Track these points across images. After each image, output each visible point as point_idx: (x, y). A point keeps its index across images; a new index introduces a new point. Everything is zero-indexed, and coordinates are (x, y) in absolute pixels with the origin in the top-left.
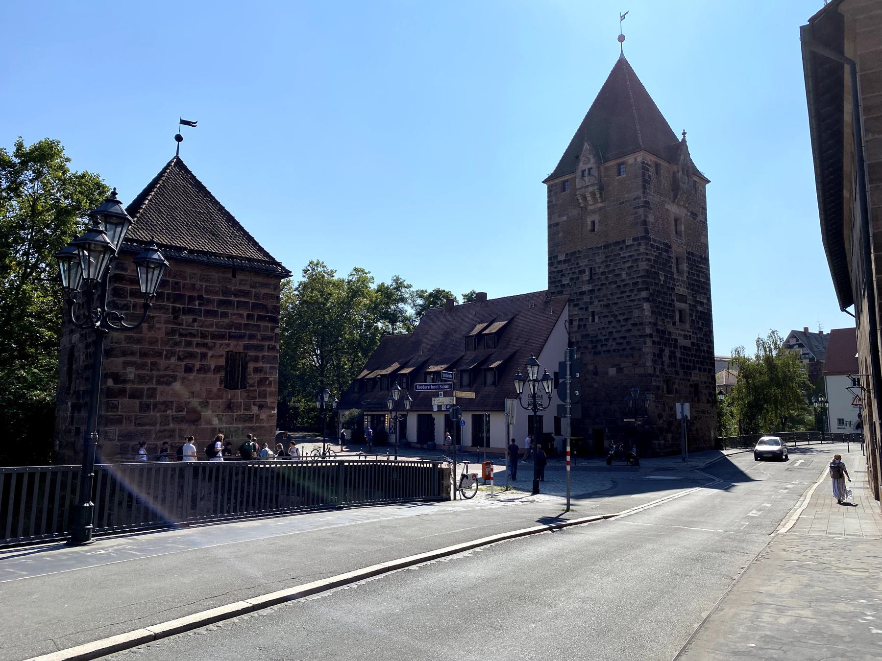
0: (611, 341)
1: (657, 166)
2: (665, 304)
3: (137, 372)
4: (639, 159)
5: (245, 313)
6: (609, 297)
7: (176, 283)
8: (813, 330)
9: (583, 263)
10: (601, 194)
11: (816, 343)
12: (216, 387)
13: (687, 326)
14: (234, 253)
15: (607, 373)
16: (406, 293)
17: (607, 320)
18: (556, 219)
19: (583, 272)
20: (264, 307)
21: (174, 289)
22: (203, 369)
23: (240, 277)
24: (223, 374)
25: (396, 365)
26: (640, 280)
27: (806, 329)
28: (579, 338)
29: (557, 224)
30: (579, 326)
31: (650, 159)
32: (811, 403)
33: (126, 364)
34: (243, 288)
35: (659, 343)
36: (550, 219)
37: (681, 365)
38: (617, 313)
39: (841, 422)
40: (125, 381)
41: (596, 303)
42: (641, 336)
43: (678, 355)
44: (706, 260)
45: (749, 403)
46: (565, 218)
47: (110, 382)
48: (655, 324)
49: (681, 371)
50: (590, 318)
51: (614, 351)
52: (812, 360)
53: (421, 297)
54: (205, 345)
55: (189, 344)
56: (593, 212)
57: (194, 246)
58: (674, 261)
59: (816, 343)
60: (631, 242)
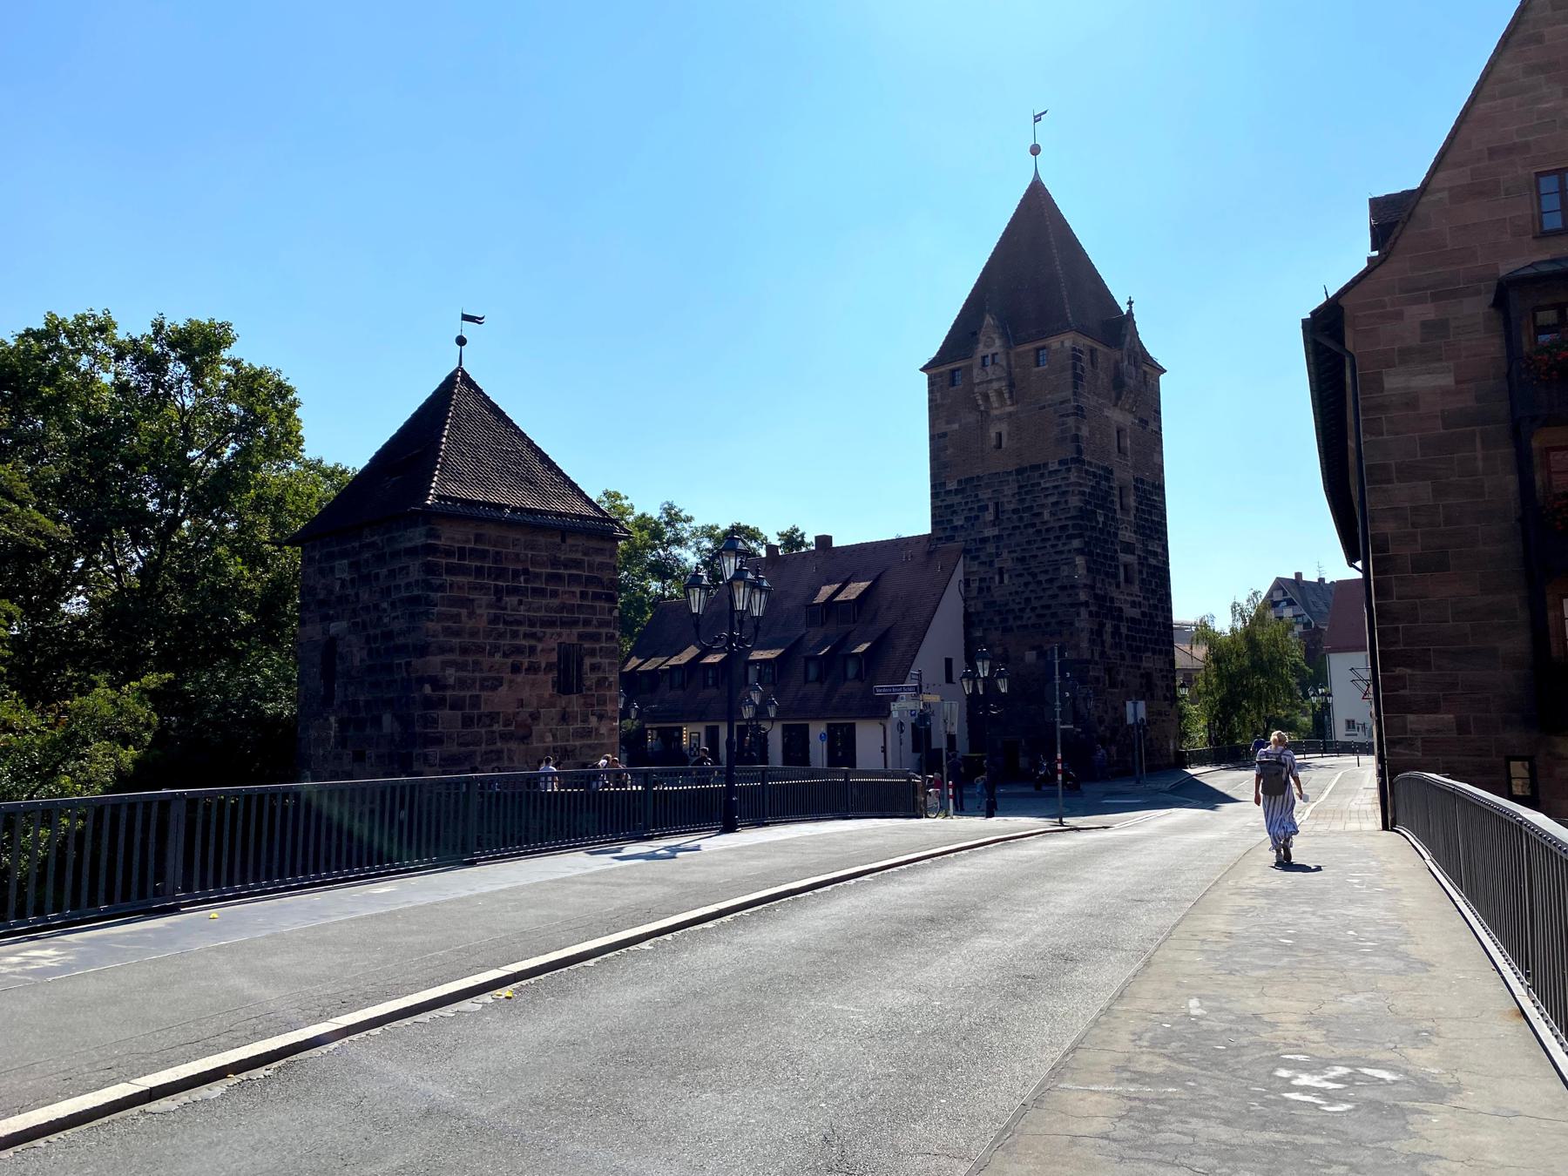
1: (1092, 351)
2: (1105, 556)
4: (1068, 344)
5: (577, 590)
7: (498, 553)
8: (1310, 576)
9: (985, 494)
10: (1011, 392)
11: (1314, 599)
12: (548, 691)
13: (1136, 588)
14: (562, 508)
15: (1022, 659)
16: (685, 530)
17: (1022, 580)
18: (944, 428)
19: (986, 508)
20: (600, 582)
21: (495, 562)
23: (570, 541)
25: (691, 652)
26: (1070, 523)
27: (1298, 575)
28: (980, 607)
29: (944, 435)
30: (980, 590)
31: (1085, 342)
32: (1306, 696)
33: (445, 664)
34: (574, 556)
35: (1098, 614)
36: (932, 426)
37: (1129, 646)
39: (1350, 724)
40: (445, 687)
41: (1005, 555)
42: (1072, 605)
43: (1124, 630)
44: (1160, 488)
45: (1221, 700)
46: (956, 426)
47: (427, 689)
48: (1093, 587)
49: (1128, 655)
51: (1033, 626)
52: (1307, 625)
53: (710, 537)
54: (533, 636)
55: (515, 635)
56: (999, 419)
57: (514, 502)
58: (1116, 492)
59: (1314, 599)
60: (1056, 467)
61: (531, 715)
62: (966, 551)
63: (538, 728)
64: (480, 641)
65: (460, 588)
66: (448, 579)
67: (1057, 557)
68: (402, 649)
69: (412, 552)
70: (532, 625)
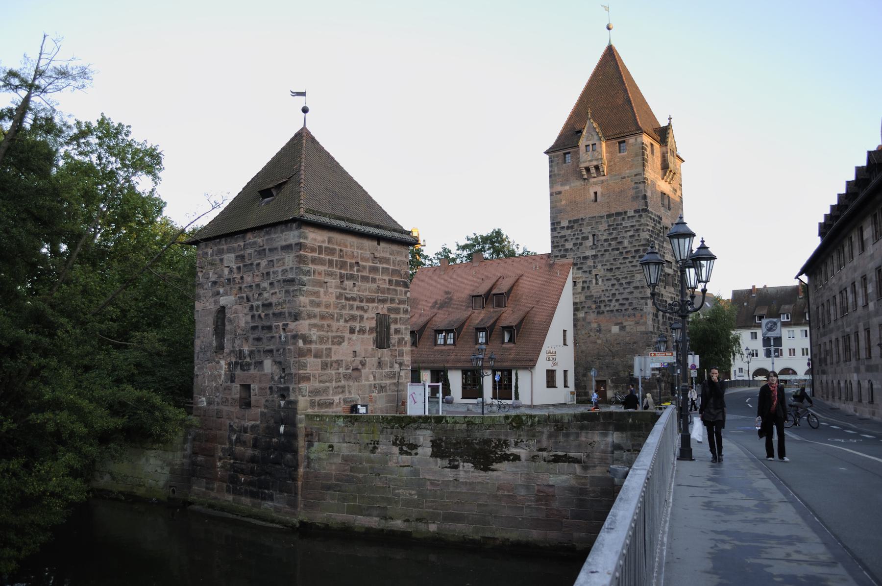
0: (614, 301)
3: (318, 333)
5: (387, 278)
6: (612, 262)
9: (586, 230)
12: (371, 346)
15: (610, 331)
17: (610, 283)
18: (559, 188)
19: (585, 238)
21: (341, 256)
22: (362, 331)
24: (375, 335)
27: (754, 287)
28: (583, 299)
30: (583, 288)
38: (620, 277)
40: (311, 342)
41: (599, 267)
42: (642, 298)
47: (300, 343)
50: (594, 281)
51: (617, 310)
54: (362, 308)
55: (351, 307)
56: (596, 184)
60: (632, 214)
61: (361, 362)
62: (575, 264)
63: (364, 371)
64: (331, 311)
65: (320, 274)
66: (312, 267)
67: (632, 269)
68: (279, 315)
69: (287, 248)
70: (361, 301)
